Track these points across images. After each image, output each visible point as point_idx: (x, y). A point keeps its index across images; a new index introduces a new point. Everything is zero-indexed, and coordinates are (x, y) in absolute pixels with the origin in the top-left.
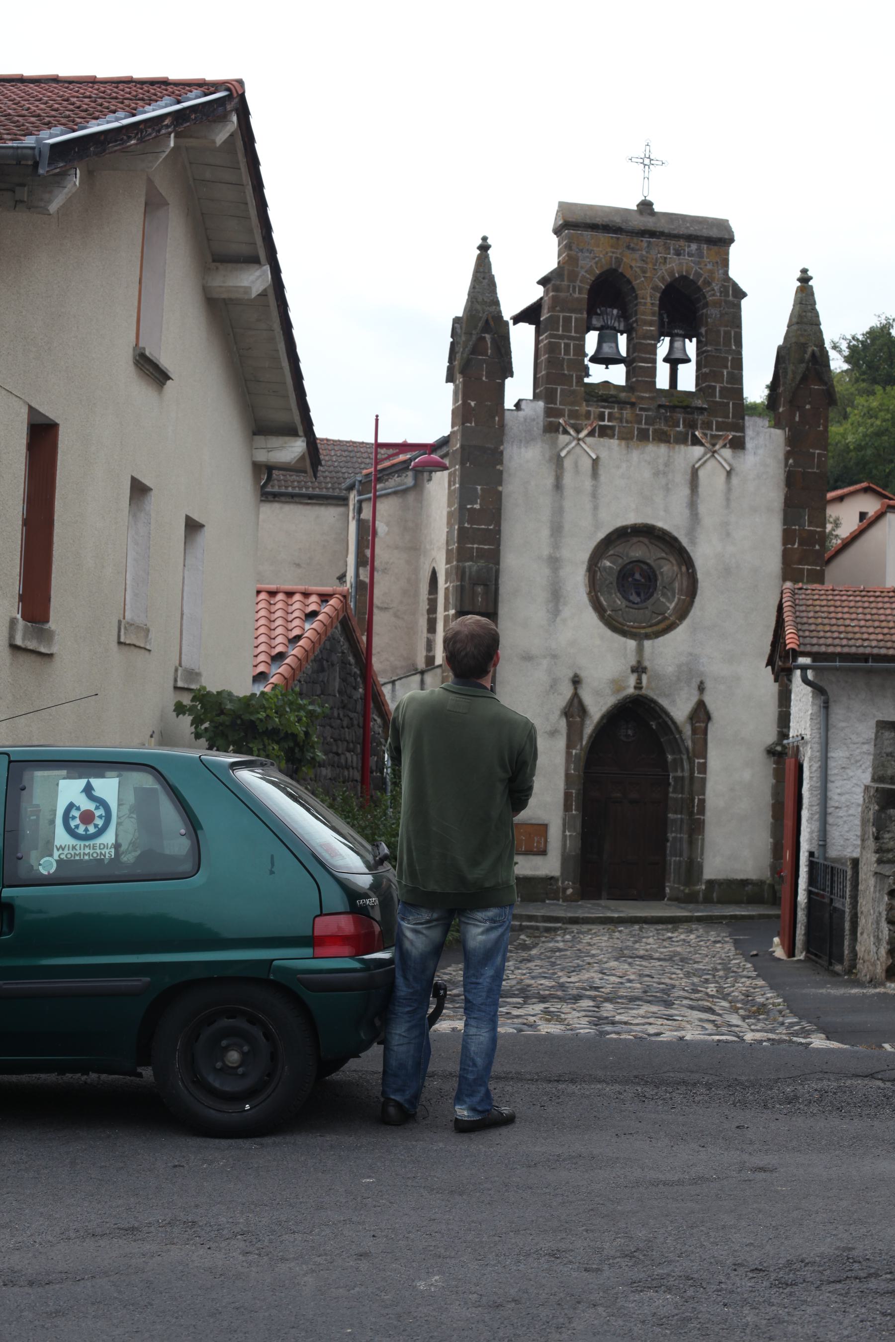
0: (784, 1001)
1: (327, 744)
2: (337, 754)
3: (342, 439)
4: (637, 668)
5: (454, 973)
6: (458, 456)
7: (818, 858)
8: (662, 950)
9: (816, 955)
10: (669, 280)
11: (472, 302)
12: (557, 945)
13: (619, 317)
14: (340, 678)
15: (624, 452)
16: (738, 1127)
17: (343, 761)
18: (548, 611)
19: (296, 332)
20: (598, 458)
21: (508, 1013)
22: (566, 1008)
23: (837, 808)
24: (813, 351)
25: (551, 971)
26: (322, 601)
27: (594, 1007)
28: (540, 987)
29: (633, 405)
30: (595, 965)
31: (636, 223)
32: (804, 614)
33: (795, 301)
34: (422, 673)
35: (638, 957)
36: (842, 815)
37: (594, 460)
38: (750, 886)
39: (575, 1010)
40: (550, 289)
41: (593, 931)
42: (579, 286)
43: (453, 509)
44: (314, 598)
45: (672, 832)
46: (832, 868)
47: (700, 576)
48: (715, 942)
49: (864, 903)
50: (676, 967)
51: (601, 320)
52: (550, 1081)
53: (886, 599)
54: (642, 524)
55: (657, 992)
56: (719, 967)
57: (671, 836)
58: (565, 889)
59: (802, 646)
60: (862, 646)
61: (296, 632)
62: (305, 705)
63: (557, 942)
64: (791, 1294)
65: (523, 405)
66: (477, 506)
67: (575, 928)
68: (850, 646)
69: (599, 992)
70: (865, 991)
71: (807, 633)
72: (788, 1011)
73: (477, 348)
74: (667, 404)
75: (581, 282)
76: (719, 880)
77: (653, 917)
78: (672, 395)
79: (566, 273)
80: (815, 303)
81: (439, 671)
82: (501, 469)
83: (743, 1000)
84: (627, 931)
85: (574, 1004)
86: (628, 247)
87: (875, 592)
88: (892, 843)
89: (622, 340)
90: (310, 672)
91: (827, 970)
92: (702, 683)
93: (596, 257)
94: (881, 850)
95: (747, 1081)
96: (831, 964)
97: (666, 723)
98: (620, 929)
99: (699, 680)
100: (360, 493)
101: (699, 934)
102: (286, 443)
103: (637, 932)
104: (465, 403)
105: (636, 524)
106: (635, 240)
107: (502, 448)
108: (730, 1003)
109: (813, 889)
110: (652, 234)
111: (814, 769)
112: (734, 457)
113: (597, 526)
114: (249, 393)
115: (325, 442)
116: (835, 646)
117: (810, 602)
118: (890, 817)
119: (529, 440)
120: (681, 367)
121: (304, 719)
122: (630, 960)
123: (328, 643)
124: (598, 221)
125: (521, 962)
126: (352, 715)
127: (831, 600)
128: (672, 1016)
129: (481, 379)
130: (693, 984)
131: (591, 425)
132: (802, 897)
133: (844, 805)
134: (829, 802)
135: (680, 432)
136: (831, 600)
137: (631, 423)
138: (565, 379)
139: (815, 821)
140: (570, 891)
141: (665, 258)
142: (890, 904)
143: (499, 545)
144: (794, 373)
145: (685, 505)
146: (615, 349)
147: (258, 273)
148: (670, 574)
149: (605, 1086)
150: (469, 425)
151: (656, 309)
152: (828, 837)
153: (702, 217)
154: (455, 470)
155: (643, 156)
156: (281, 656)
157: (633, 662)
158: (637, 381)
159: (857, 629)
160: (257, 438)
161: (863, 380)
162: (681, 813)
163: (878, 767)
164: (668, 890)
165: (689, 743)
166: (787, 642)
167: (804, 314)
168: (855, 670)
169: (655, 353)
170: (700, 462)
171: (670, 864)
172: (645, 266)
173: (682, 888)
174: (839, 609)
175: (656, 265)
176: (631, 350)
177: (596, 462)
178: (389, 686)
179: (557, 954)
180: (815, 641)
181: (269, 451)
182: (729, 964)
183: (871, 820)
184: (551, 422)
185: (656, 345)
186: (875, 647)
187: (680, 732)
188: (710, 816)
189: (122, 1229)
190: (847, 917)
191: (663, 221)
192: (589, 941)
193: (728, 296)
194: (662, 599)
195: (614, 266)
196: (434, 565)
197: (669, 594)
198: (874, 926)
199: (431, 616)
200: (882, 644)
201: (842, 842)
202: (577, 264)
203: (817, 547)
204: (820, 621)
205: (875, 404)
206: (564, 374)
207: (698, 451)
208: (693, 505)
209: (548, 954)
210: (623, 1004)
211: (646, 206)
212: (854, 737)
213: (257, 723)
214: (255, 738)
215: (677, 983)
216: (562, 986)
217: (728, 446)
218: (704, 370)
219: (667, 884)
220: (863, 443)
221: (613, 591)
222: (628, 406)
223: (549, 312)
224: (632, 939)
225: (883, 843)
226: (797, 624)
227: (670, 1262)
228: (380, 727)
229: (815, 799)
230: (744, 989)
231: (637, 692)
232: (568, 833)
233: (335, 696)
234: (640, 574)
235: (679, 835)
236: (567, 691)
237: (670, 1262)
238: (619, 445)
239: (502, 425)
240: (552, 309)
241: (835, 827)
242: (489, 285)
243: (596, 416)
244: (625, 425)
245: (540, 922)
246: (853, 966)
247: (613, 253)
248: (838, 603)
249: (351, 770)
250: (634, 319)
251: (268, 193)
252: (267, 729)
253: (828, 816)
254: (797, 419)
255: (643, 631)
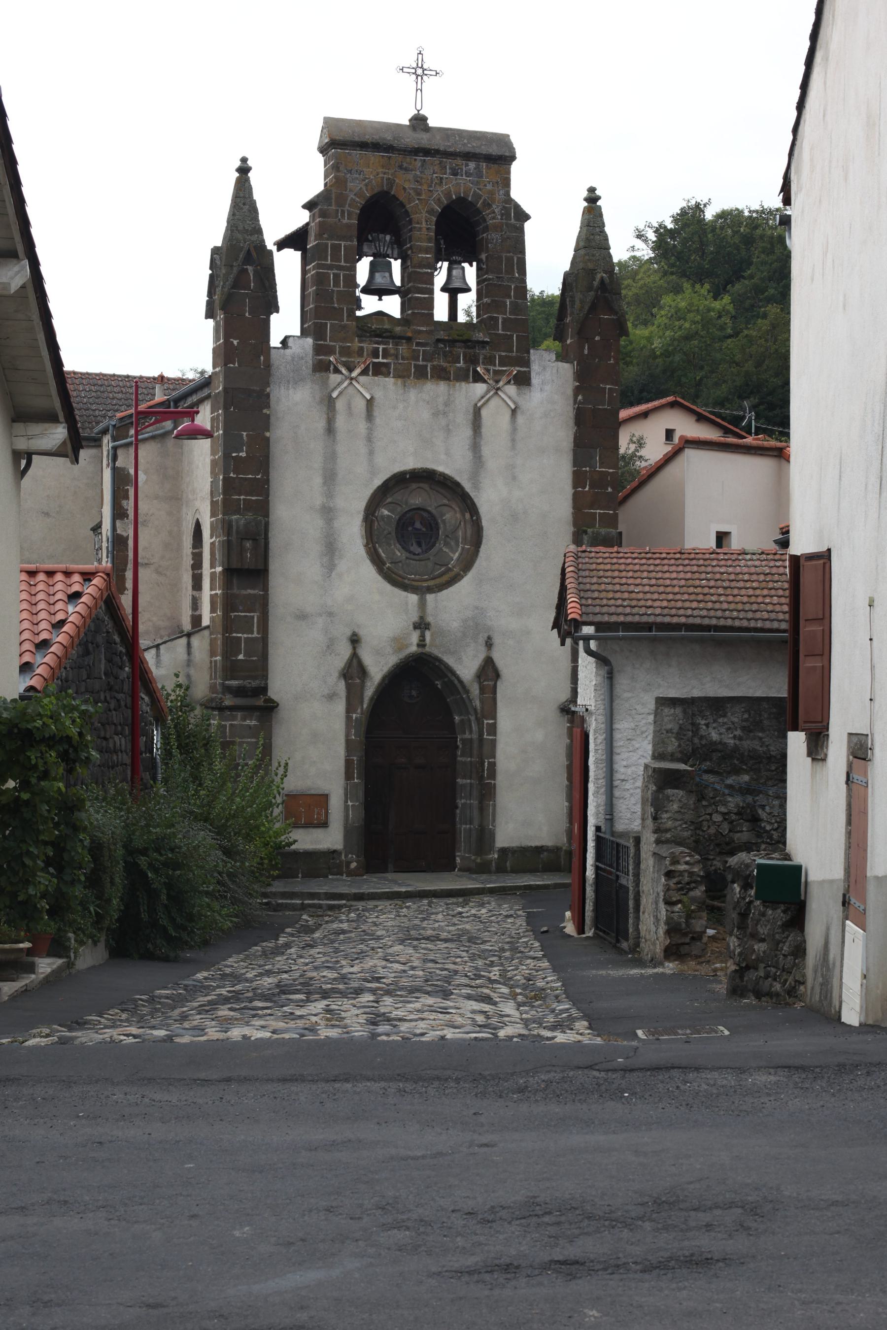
0: (563, 985)
1: (95, 729)
2: (105, 739)
3: (90, 371)
4: (420, 624)
5: (236, 965)
6: (222, 400)
7: (605, 833)
8: (450, 928)
9: (604, 932)
10: (446, 202)
11: (232, 231)
12: (341, 925)
13: (391, 243)
14: (105, 659)
15: (401, 391)
16: (475, 1114)
17: (111, 745)
18: (322, 565)
19: (56, 323)
20: (372, 398)
21: (292, 1014)
22: (346, 1004)
23: (623, 780)
24: (602, 277)
25: (334, 959)
26: (85, 580)
27: (373, 1001)
28: (323, 979)
29: (409, 339)
30: (379, 950)
31: (408, 140)
32: (588, 580)
33: (582, 223)
34: (189, 635)
35: (424, 938)
36: (628, 788)
37: (368, 401)
38: (545, 853)
39: (355, 1006)
40: (317, 215)
41: (380, 908)
42: (348, 210)
43: (217, 457)
44: (76, 578)
45: (461, 798)
46: (618, 844)
47: (484, 523)
48: (507, 917)
49: (645, 882)
50: (462, 949)
51: (373, 247)
52: (328, 1081)
53: (673, 562)
54: (422, 468)
55: (438, 980)
56: (507, 946)
57: (460, 802)
58: (348, 863)
59: (584, 616)
60: (646, 614)
61: (60, 616)
62: (78, 705)
63: (341, 922)
64: (490, 1228)
65: (290, 342)
66: (243, 454)
67: (360, 905)
68: (634, 615)
69: (380, 983)
70: (643, 972)
71: (590, 601)
72: (564, 996)
73: (239, 282)
74: (446, 338)
75: (350, 206)
76: (513, 848)
77: (442, 890)
78: (452, 328)
79: (333, 196)
80: (603, 225)
81: (206, 633)
82: (268, 412)
83: (524, 984)
84: (415, 906)
85: (355, 998)
86: (401, 167)
87: (661, 553)
88: (670, 823)
89: (396, 266)
90: (75, 657)
91: (615, 946)
92: (489, 638)
93: (367, 178)
94: (660, 830)
95: (489, 1075)
96: (618, 941)
97: (452, 682)
98: (407, 904)
99: (486, 635)
100: (114, 439)
101: (491, 908)
102: (46, 430)
103: (426, 907)
104: (227, 342)
105: (415, 469)
106: (408, 159)
107: (268, 390)
108: (511, 988)
109: (600, 865)
110: (427, 152)
111: (599, 741)
112: (519, 394)
113: (373, 473)
114: (7, 381)
115: (73, 375)
116: (618, 614)
117: (594, 566)
118: (668, 797)
119: (297, 380)
120: (461, 297)
121: (78, 720)
122: (415, 943)
123: (92, 625)
124: (368, 138)
125: (303, 948)
126: (120, 696)
127: (615, 564)
128: (446, 1009)
129: (245, 315)
130: (476, 969)
131: (364, 362)
132: (590, 873)
133: (630, 778)
134: (615, 774)
135: (460, 369)
136: (615, 564)
137: (408, 359)
138: (335, 314)
139: (601, 794)
140: (353, 865)
141: (441, 179)
142: (667, 885)
143: (268, 495)
144: (582, 302)
145: (467, 447)
146: (388, 278)
147: (16, 268)
148: (453, 522)
149: (373, 1083)
150: (232, 365)
151: (433, 234)
152: (614, 810)
153: (480, 132)
154: (218, 415)
155: (415, 65)
156: (43, 645)
157: (415, 618)
158: (413, 313)
159: (641, 596)
160: (15, 424)
161: (672, 273)
162: (471, 778)
163: (658, 744)
164: (458, 860)
165: (477, 703)
166: (569, 611)
167: (592, 237)
168: (639, 639)
169: (432, 283)
170: (483, 401)
171: (461, 833)
172: (420, 187)
173: (473, 857)
174: (624, 574)
175: (431, 186)
176: (406, 279)
177: (370, 403)
178: (153, 651)
179: (342, 937)
180: (597, 610)
181: (29, 439)
182: (518, 942)
183: (650, 800)
184: (321, 360)
185: (433, 273)
186: (659, 615)
187: (467, 692)
188: (501, 780)
189: (14, 1208)
190: (631, 895)
191: (438, 138)
192: (375, 920)
193: (511, 220)
194: (445, 549)
195: (385, 188)
196: (197, 516)
197: (453, 543)
198: (654, 906)
199: (196, 572)
200: (666, 611)
201: (629, 816)
202: (346, 187)
203: (610, 490)
204: (603, 587)
205: (683, 304)
206: (335, 308)
207: (480, 388)
208: (476, 447)
209: (332, 937)
210: (401, 996)
211: (419, 121)
212: (638, 707)
213: (34, 731)
214: (32, 746)
215: (460, 968)
216: (343, 978)
217: (512, 382)
218: (485, 300)
219: (458, 854)
220: (671, 348)
221: (392, 542)
222: (404, 341)
223: (315, 240)
224: (420, 916)
225: (662, 823)
226: (580, 591)
227: (409, 1211)
228: (148, 705)
229: (600, 772)
230: (527, 972)
231: (420, 650)
232: (350, 803)
233: (101, 678)
234: (421, 523)
235: (468, 802)
236: (345, 651)
237: (409, 1211)
238: (395, 384)
239: (268, 365)
240: (319, 236)
241: (621, 801)
242: (250, 211)
243: (370, 352)
244: (400, 361)
245: (323, 900)
246: (637, 945)
247: (385, 173)
248: (622, 567)
249: (120, 753)
250: (408, 246)
251: (26, 191)
252: (44, 736)
253: (614, 789)
254: (586, 352)
255: (425, 584)
